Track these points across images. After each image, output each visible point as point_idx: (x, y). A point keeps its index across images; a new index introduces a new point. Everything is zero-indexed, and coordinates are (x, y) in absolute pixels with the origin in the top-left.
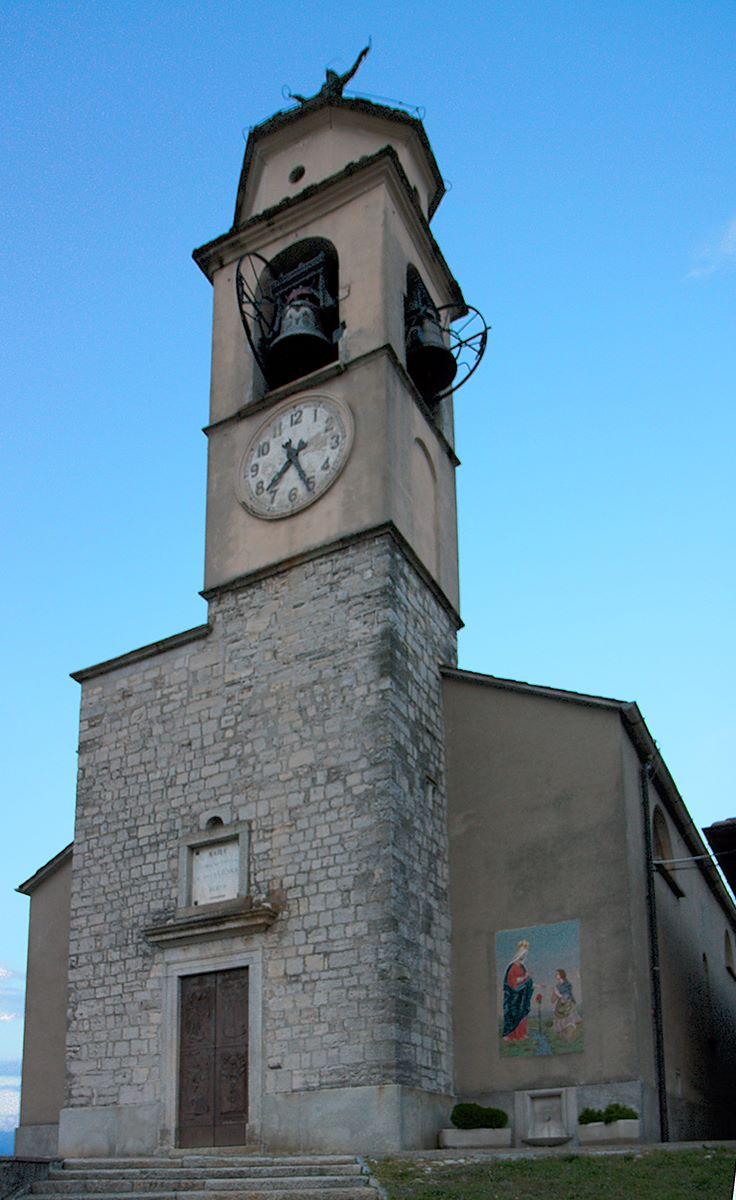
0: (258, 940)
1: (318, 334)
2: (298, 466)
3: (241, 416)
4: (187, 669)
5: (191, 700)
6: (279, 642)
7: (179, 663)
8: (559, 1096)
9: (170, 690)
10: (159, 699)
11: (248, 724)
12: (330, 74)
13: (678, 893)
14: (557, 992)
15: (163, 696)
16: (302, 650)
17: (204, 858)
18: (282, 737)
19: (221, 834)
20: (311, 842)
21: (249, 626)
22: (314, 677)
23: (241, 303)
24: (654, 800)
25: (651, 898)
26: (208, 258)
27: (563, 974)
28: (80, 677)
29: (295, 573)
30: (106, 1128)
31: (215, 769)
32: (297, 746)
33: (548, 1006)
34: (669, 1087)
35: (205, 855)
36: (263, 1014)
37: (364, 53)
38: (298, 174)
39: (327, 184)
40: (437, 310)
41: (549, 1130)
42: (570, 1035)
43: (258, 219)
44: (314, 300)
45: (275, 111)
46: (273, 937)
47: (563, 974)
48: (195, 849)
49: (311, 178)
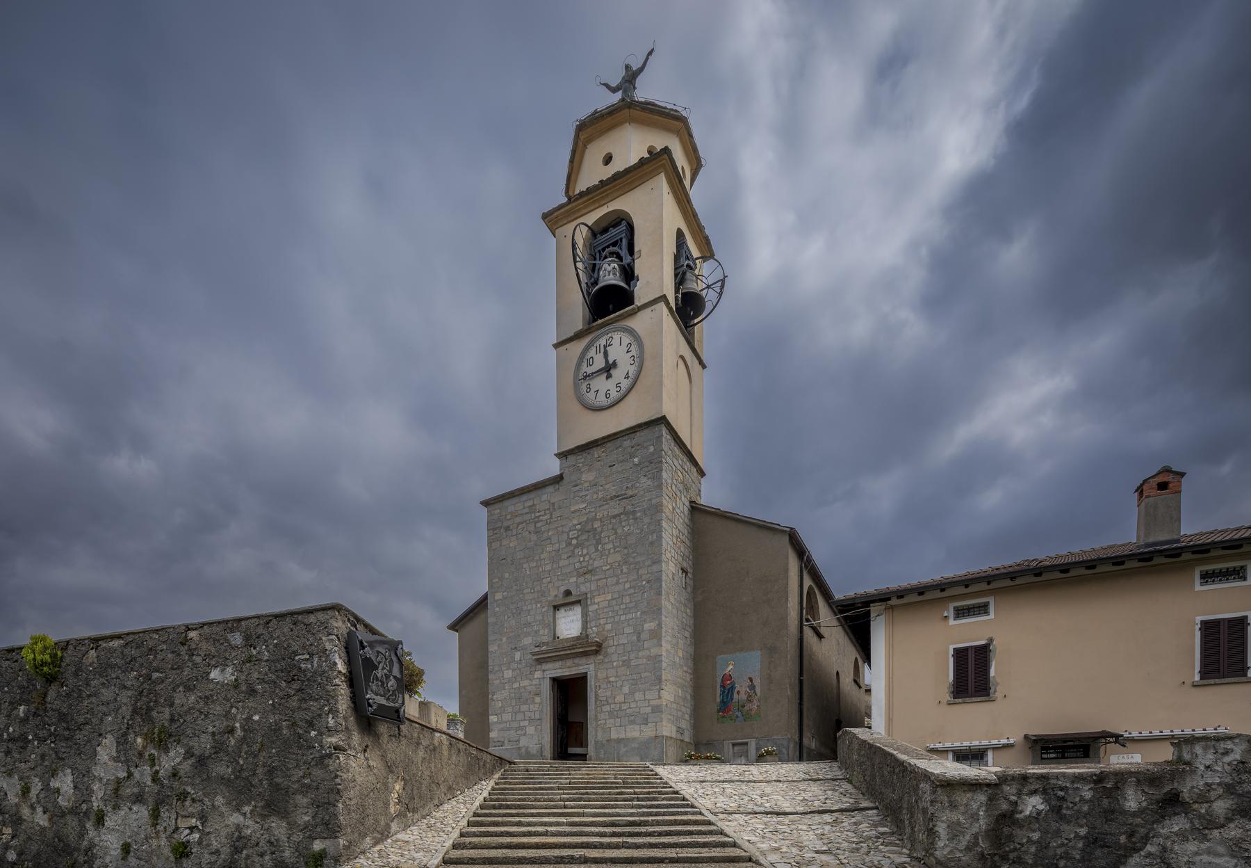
0: (592, 659)
1: (623, 284)
2: (607, 361)
3: (578, 336)
7: (544, 497)
8: (746, 744)
12: (627, 67)
13: (820, 636)
17: (561, 614)
21: (584, 477)
23: (575, 262)
24: (808, 582)
25: (801, 640)
26: (553, 219)
27: (751, 679)
28: (486, 503)
29: (609, 445)
31: (567, 562)
33: (743, 696)
34: (805, 741)
35: (562, 610)
37: (650, 53)
38: (608, 159)
39: (628, 171)
40: (694, 260)
43: (582, 194)
44: (620, 258)
45: (592, 110)
46: (600, 657)
47: (751, 679)
48: (556, 608)
49: (618, 165)
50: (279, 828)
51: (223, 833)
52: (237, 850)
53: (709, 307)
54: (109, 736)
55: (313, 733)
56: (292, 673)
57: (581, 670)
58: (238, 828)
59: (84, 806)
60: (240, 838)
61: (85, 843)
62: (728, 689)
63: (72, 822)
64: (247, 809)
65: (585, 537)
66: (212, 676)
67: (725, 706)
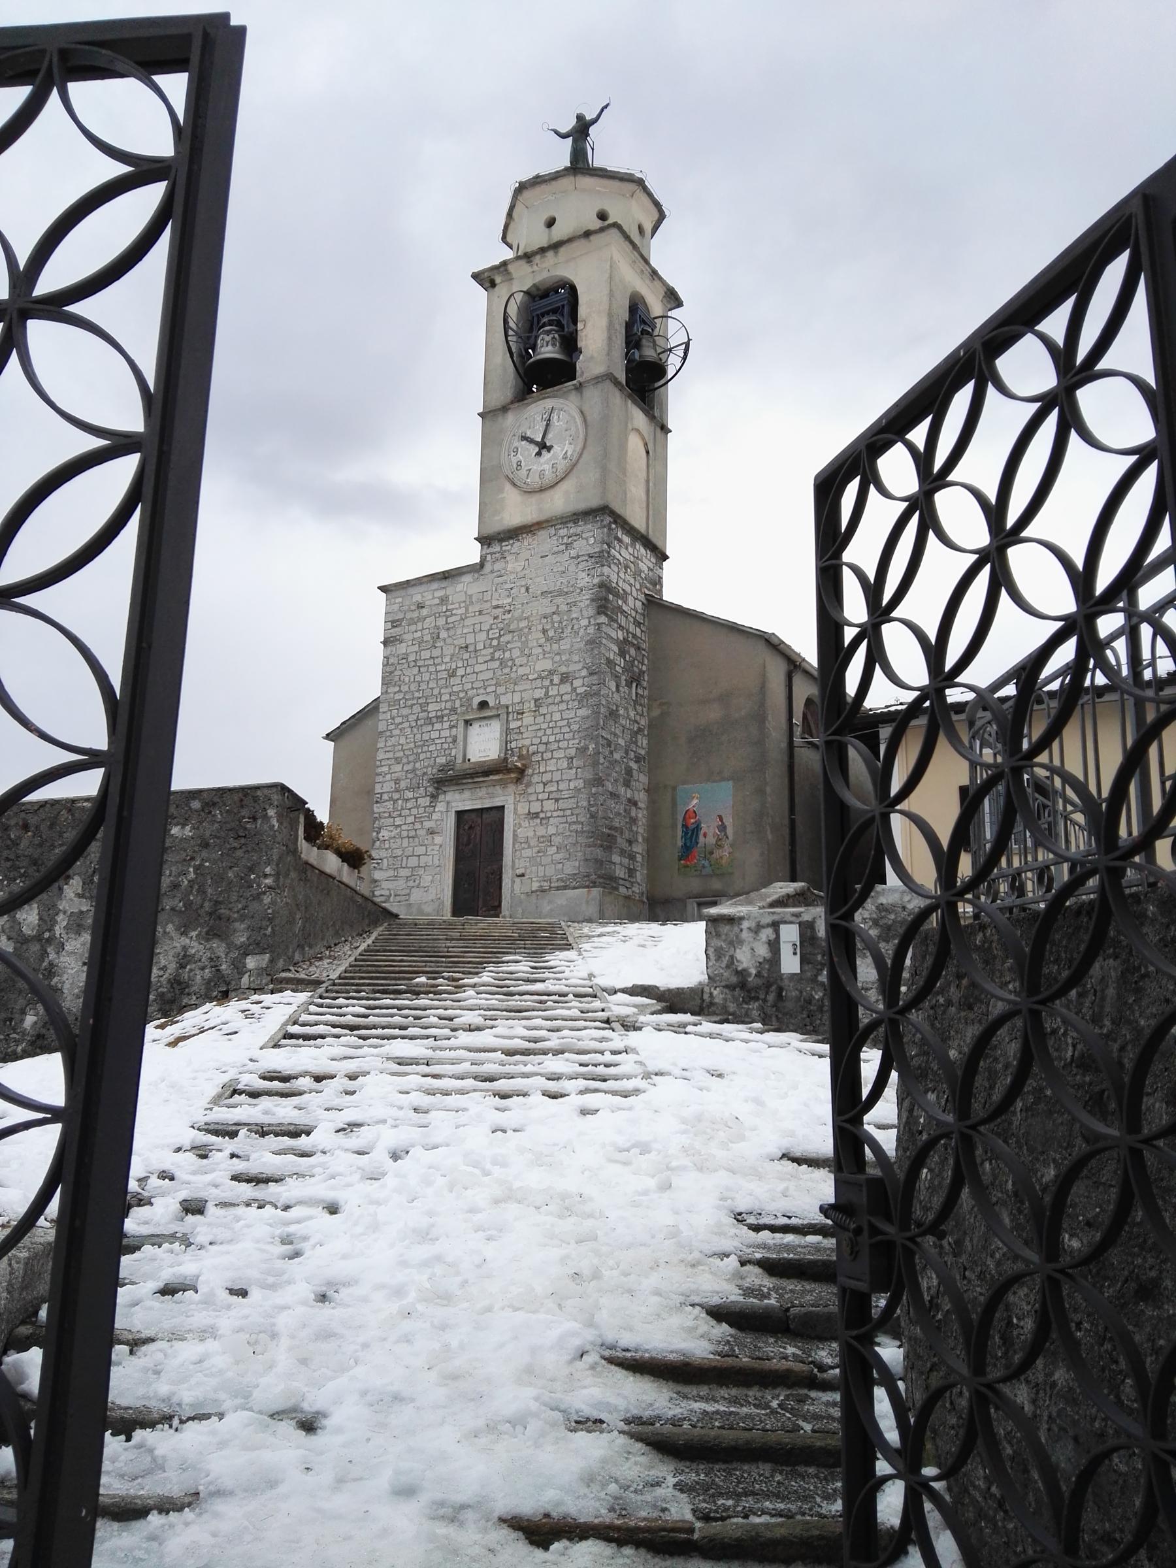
7: (460, 587)
16: (546, 589)
17: (475, 730)
32: (541, 656)
33: (711, 840)
35: (476, 726)
37: (606, 107)
50: (219, 947)
51: (171, 953)
52: (182, 966)
53: (671, 372)
54: (77, 878)
55: (252, 876)
56: (241, 834)
57: (497, 802)
58: (185, 948)
59: (47, 935)
60: (185, 956)
61: (45, 964)
62: (692, 833)
63: (35, 948)
64: (194, 934)
65: (508, 637)
66: (173, 832)
67: (687, 850)
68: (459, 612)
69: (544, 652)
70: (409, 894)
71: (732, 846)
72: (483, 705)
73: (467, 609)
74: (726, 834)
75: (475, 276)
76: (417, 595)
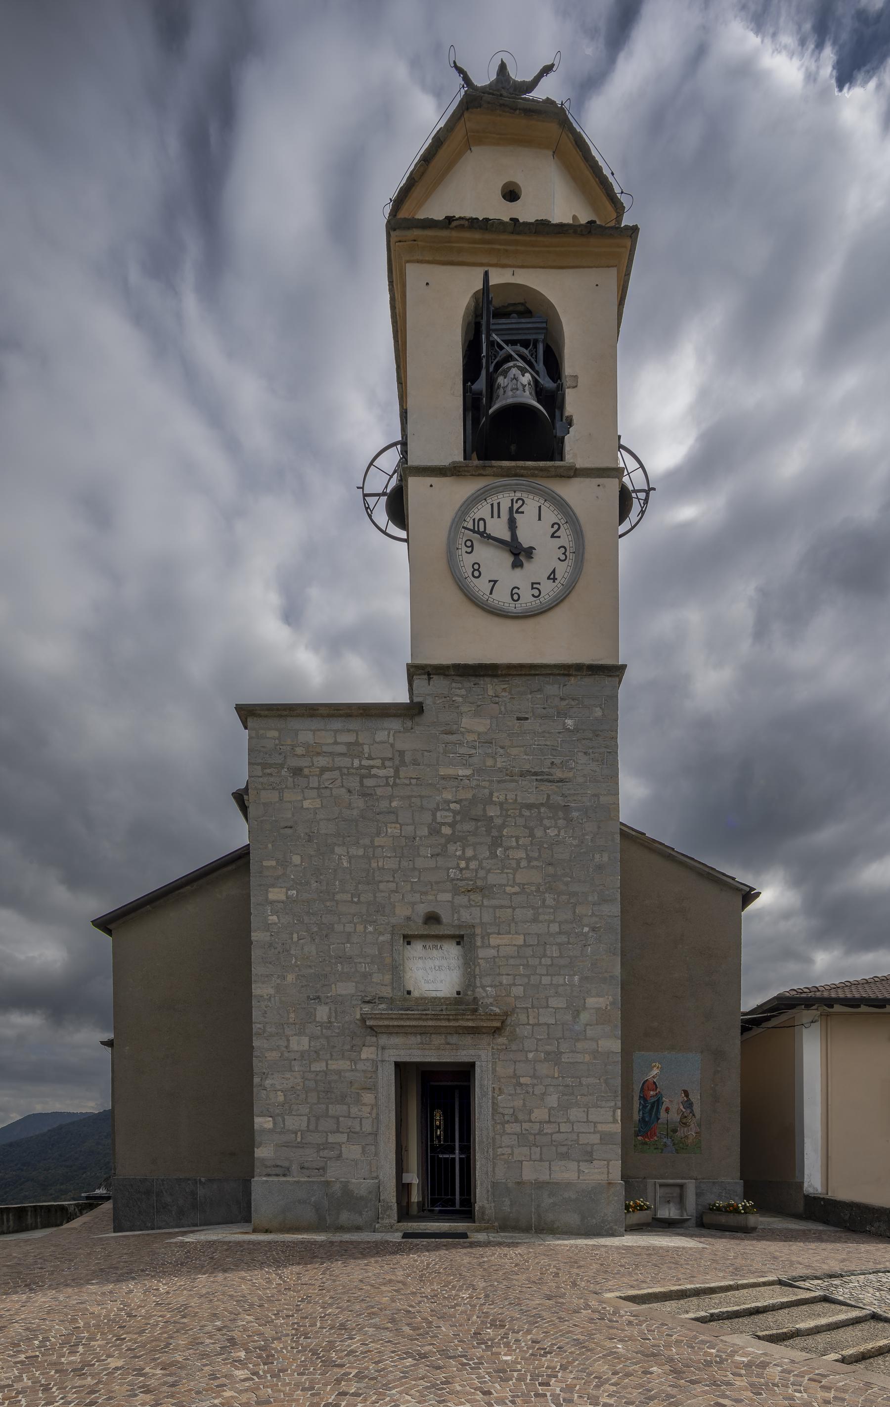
4: (392, 745)
5: (398, 781)
6: (501, 751)
7: (381, 736)
9: (371, 762)
10: (357, 769)
11: (468, 826)
14: (682, 1107)
15: (361, 767)
16: (527, 767)
18: (507, 849)
19: (435, 930)
20: (541, 958)
22: (543, 799)
27: (686, 1093)
29: (517, 681)
30: (313, 1199)
31: (432, 863)
32: (524, 863)
33: (674, 1117)
36: (493, 1108)
41: (669, 1210)
42: (690, 1141)
47: (686, 1093)
57: (463, 1056)
68: (381, 773)
69: (529, 859)
70: (324, 1169)
71: (699, 1125)
72: (432, 918)
73: (397, 771)
74: (692, 1112)
75: (102, 1043)
76: (307, 733)
